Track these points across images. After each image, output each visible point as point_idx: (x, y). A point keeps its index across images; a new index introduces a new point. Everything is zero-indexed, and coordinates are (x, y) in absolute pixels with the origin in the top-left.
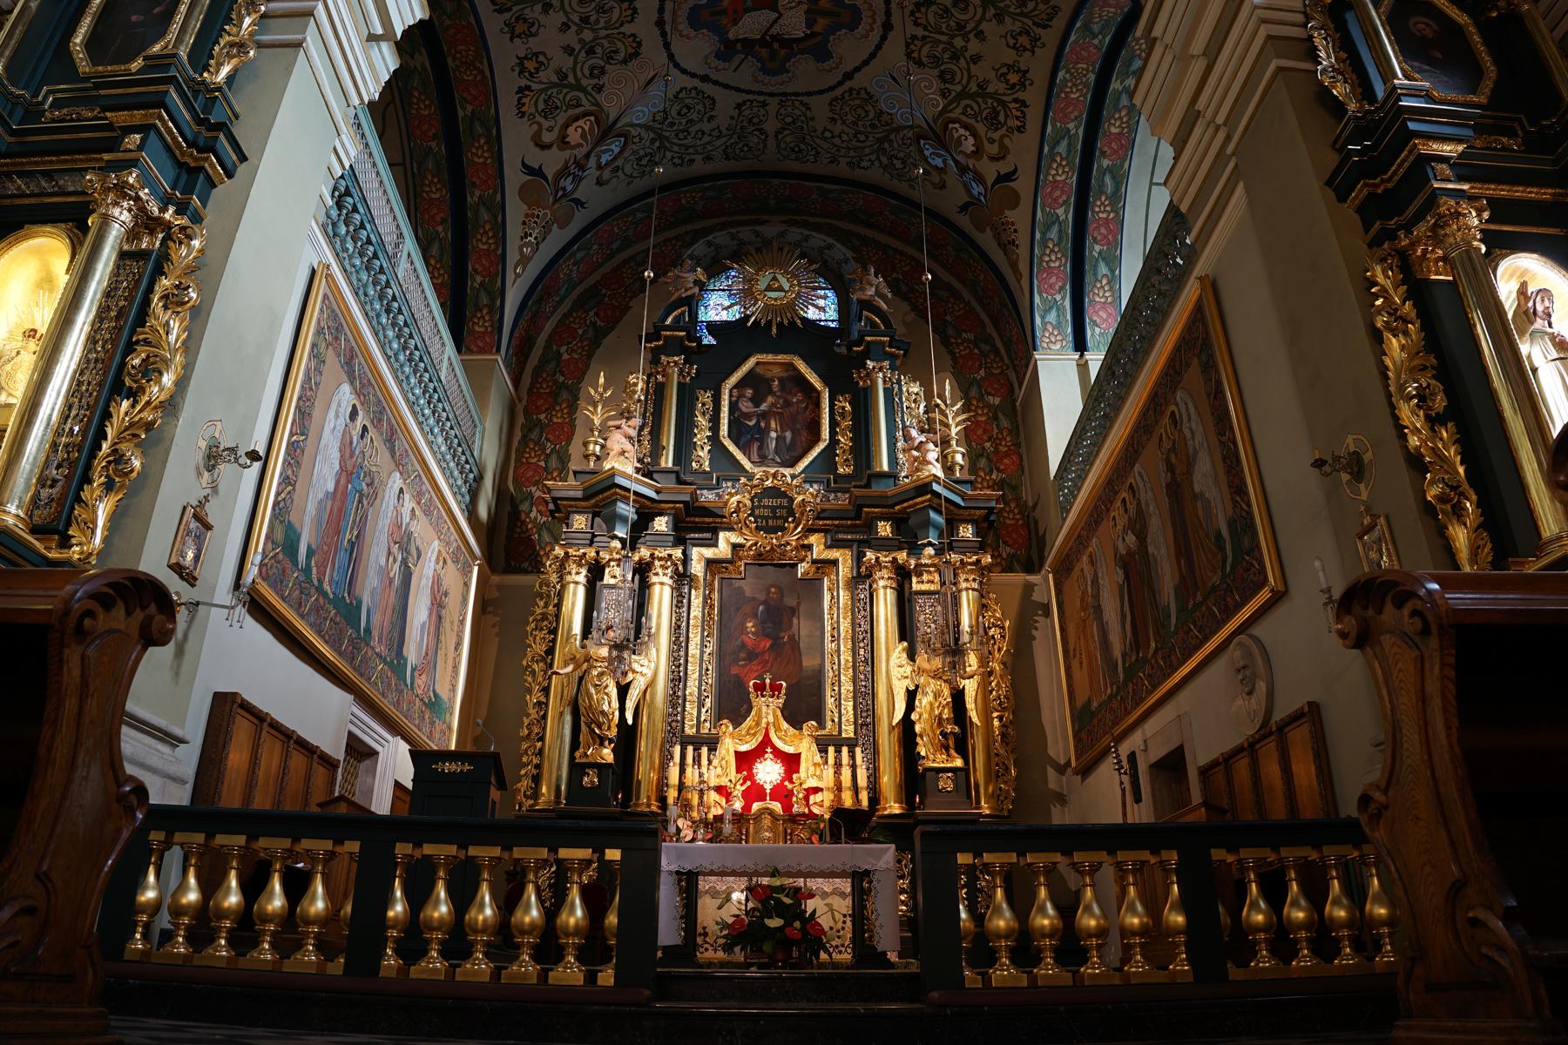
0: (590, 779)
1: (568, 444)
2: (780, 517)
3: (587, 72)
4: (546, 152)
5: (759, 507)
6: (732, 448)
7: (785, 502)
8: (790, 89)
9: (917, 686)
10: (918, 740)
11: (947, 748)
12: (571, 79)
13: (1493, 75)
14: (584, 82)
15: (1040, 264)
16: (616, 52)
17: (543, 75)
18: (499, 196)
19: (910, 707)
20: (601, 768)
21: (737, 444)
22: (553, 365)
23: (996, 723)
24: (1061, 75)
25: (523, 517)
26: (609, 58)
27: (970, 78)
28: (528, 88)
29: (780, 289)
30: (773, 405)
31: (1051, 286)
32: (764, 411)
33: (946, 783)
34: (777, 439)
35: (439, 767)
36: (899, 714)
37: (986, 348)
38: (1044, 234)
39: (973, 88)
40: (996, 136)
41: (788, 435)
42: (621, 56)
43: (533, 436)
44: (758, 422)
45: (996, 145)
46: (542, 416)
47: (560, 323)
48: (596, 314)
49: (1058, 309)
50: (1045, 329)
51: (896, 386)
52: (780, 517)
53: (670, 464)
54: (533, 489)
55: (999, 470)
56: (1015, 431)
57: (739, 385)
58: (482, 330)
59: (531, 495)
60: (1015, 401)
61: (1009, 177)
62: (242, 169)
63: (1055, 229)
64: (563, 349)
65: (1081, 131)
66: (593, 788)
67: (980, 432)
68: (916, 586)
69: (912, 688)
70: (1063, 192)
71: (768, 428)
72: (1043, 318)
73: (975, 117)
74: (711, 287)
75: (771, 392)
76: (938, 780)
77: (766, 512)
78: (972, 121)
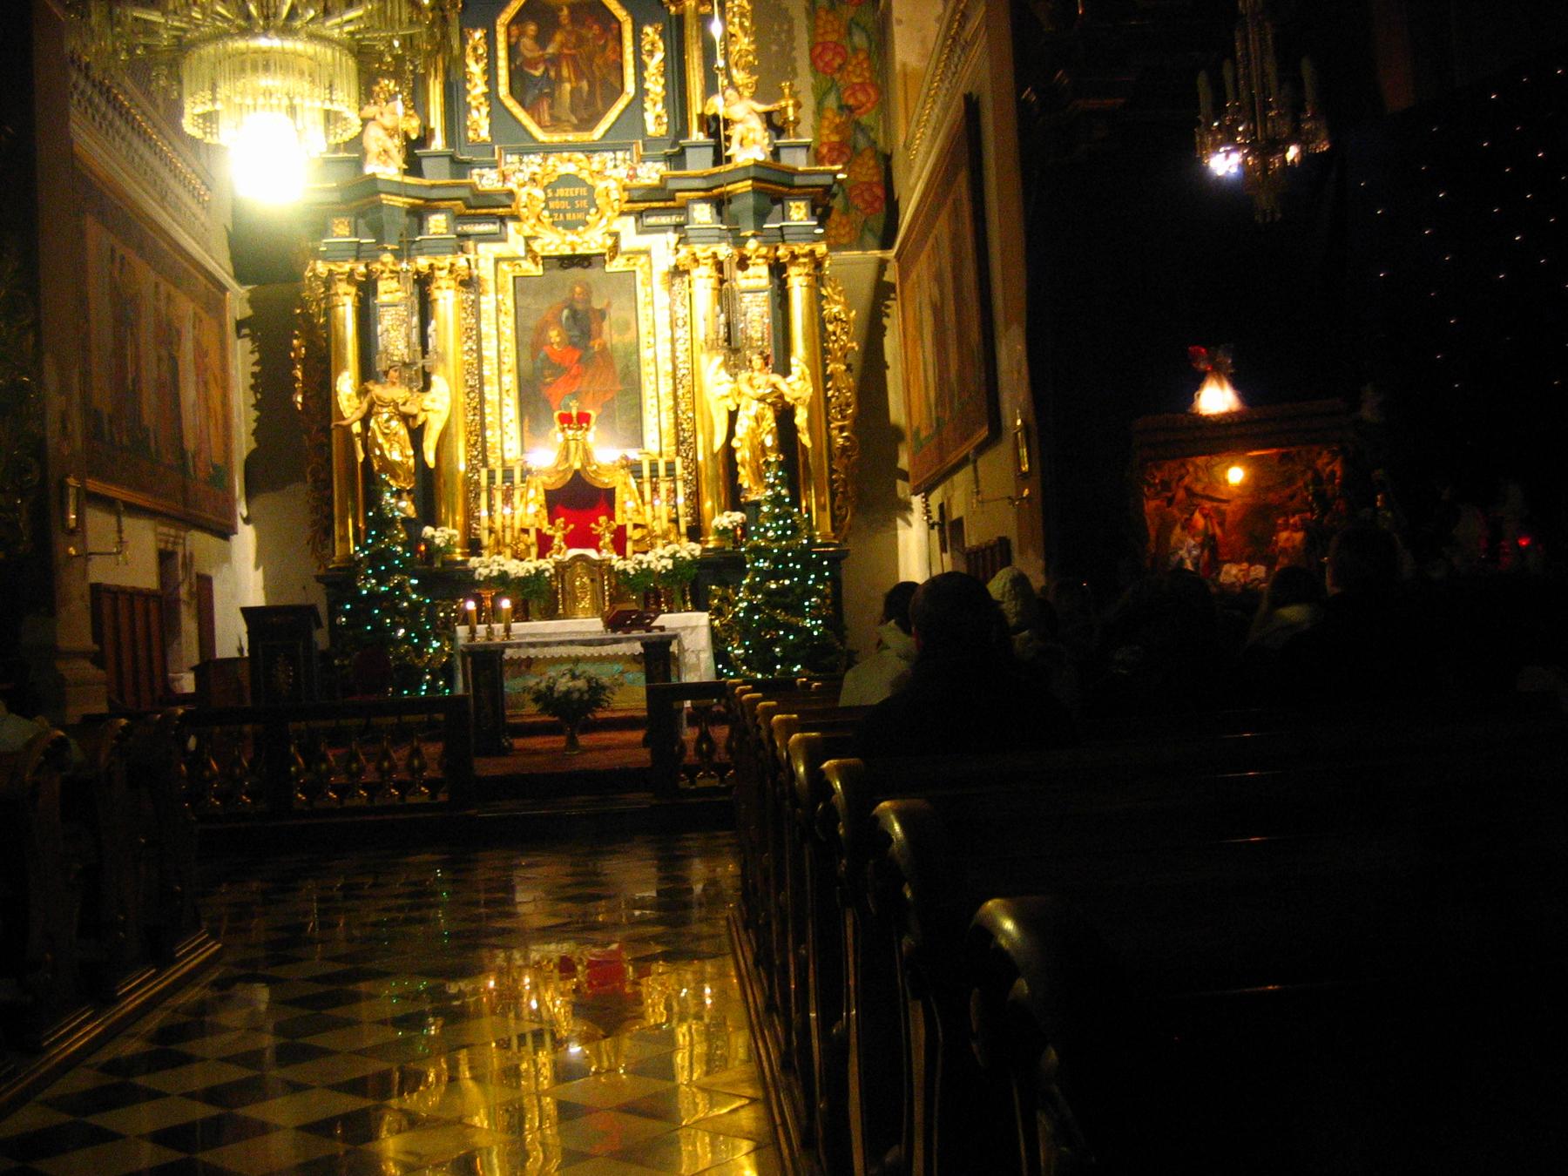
2: (580, 210)
5: (554, 198)
7: (584, 191)
9: (738, 406)
10: (740, 469)
19: (731, 433)
21: (522, 104)
30: (563, 45)
32: (553, 54)
34: (572, 92)
35: (1202, 80)
41: (585, 85)
44: (547, 71)
52: (580, 210)
53: (563, 738)
69: (733, 408)
77: (564, 204)
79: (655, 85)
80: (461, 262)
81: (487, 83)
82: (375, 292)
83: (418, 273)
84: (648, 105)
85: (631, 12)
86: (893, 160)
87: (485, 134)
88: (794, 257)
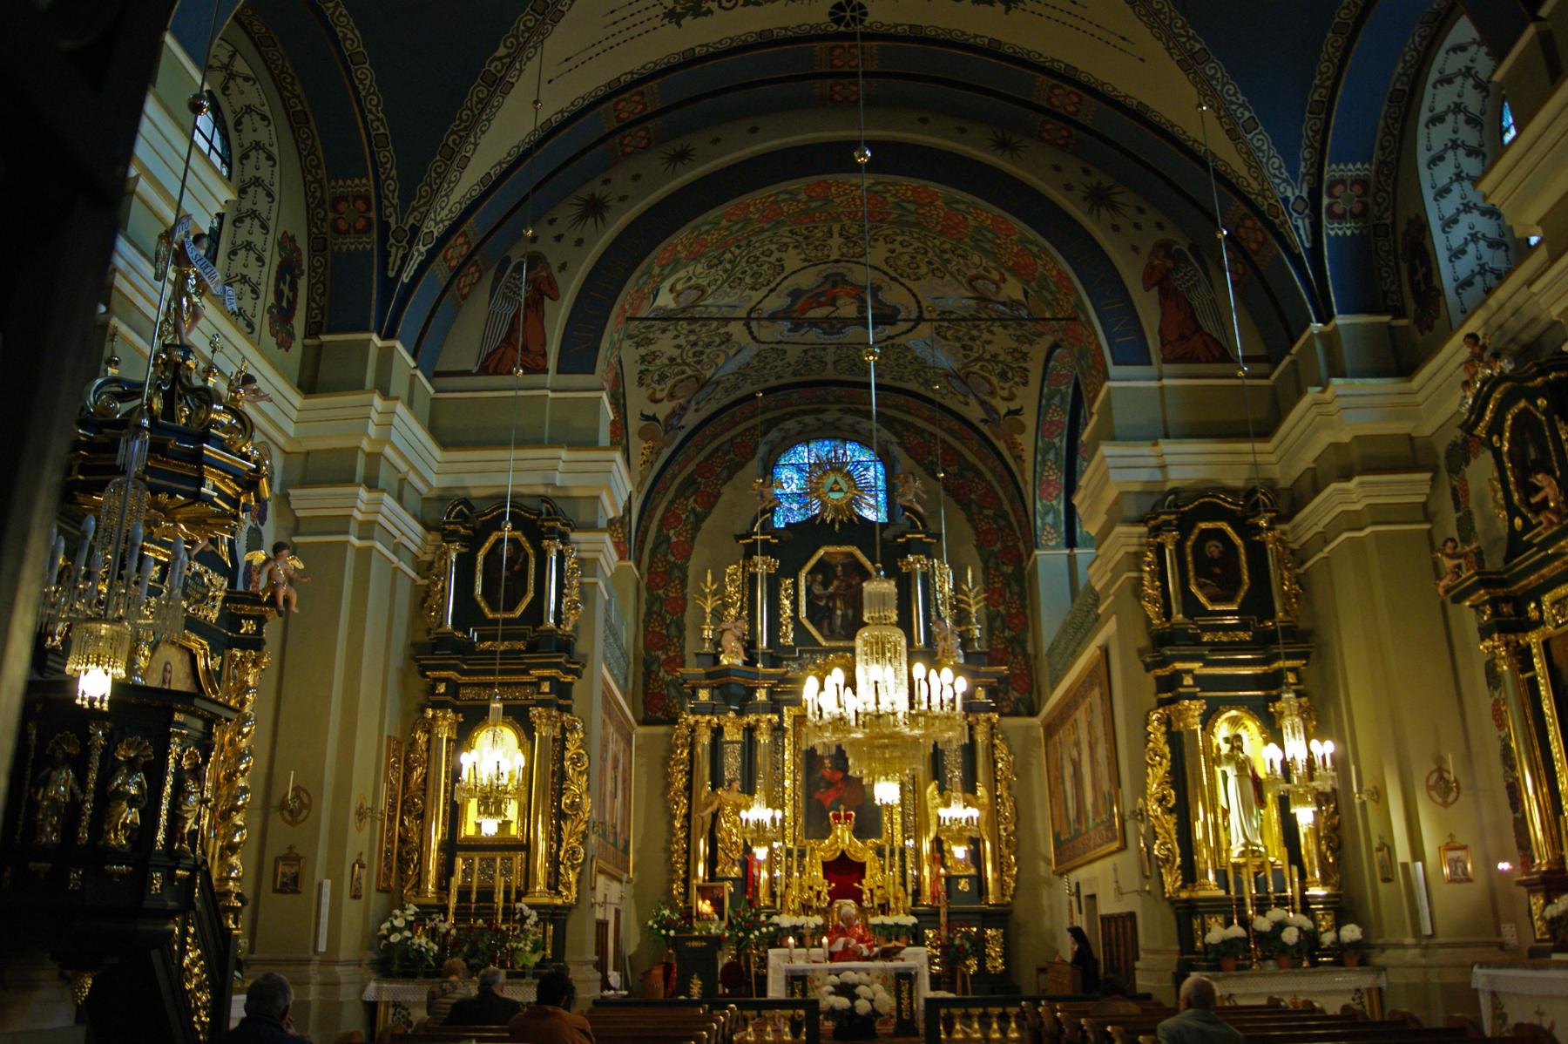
8: (845, 341)
12: (679, 360)
13: (1246, 587)
14: (688, 361)
17: (658, 362)
22: (665, 546)
24: (1052, 364)
26: (708, 345)
29: (840, 490)
30: (838, 588)
31: (1050, 494)
35: (689, 944)
37: (1002, 523)
38: (1043, 457)
40: (1007, 386)
46: (661, 592)
47: (667, 510)
48: (695, 501)
50: (1044, 529)
54: (660, 653)
55: (1010, 629)
56: (1022, 595)
57: (811, 572)
62: (585, 672)
64: (672, 533)
65: (1070, 390)
71: (834, 609)
72: (1042, 519)
73: (990, 372)
74: (782, 462)
75: (836, 577)
76: (958, 884)
81: (792, 611)
83: (748, 724)
87: (790, 641)
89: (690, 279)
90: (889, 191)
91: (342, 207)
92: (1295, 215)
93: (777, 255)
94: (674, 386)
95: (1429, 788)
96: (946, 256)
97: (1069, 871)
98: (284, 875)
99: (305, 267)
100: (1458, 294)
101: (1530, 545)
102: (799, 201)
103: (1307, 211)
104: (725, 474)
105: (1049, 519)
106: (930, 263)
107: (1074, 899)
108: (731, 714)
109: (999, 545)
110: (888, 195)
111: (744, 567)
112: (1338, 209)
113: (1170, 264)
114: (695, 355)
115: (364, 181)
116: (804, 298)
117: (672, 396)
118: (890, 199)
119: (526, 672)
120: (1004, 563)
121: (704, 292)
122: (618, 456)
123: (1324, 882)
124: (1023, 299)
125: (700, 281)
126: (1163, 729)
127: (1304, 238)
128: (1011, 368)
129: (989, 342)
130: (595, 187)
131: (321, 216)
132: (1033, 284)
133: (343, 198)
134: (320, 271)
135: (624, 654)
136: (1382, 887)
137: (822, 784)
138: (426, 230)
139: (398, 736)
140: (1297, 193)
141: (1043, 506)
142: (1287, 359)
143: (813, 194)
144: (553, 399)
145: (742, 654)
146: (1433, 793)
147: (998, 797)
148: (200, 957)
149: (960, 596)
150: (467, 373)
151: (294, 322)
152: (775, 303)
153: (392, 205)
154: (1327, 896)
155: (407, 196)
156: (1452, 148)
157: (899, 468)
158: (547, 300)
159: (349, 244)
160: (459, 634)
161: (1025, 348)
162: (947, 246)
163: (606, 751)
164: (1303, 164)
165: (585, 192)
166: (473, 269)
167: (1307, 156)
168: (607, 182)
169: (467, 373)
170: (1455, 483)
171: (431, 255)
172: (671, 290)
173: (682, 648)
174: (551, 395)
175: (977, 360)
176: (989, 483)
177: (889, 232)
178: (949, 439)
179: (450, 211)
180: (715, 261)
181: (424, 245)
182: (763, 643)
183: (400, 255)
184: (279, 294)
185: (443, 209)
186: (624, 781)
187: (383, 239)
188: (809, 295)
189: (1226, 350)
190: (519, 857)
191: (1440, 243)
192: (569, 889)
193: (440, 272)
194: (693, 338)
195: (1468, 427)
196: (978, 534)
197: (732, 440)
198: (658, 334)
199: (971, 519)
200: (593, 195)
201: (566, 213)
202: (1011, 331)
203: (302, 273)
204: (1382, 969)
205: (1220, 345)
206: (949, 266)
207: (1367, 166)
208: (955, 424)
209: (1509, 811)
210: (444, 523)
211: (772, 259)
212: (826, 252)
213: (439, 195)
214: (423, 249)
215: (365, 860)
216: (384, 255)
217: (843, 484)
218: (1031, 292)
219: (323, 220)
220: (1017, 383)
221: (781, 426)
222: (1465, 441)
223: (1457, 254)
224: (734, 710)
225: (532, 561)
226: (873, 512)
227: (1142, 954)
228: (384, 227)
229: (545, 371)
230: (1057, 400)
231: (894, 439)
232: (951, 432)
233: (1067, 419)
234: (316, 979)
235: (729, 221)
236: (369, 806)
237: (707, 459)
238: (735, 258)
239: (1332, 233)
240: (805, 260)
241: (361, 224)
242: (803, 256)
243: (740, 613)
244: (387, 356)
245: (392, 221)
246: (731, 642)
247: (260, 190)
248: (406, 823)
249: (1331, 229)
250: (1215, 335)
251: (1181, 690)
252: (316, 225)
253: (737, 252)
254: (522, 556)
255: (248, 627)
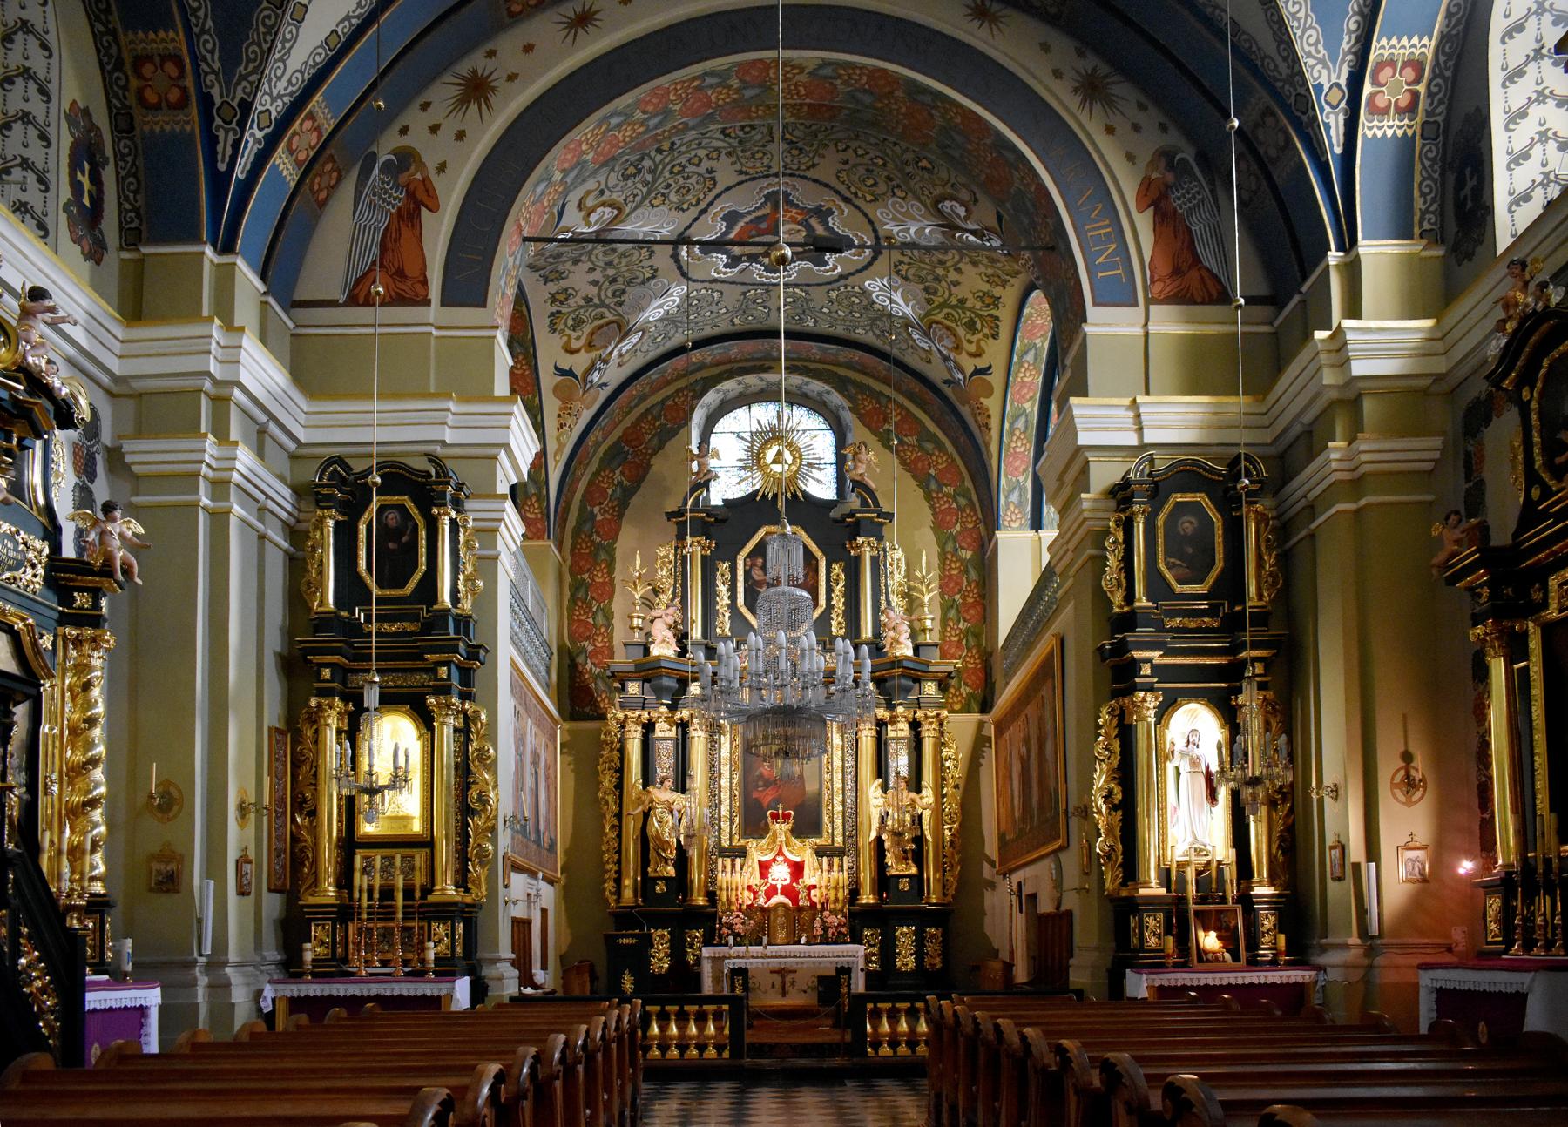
0: (660, 888)
1: (611, 602)
3: (610, 294)
4: (576, 356)
6: (744, 610)
11: (906, 859)
12: (596, 301)
14: (607, 301)
15: (1007, 450)
16: (636, 278)
17: (571, 302)
18: (537, 399)
20: (667, 880)
22: (588, 527)
23: (947, 833)
25: (580, 668)
26: (629, 283)
27: (950, 295)
28: (559, 312)
31: (1016, 469)
33: (904, 885)
36: (873, 835)
37: (963, 501)
38: (1012, 424)
39: (954, 302)
40: (974, 338)
42: (639, 281)
43: (580, 595)
45: (974, 345)
46: (586, 576)
47: (591, 483)
48: (622, 473)
49: (1021, 489)
50: (1008, 508)
51: (882, 553)
54: (586, 643)
55: (965, 620)
58: (533, 516)
59: (584, 649)
60: (985, 554)
61: (984, 371)
63: (1022, 420)
64: (596, 509)
65: (1046, 345)
66: (663, 894)
67: (951, 585)
68: (891, 734)
70: (1030, 389)
72: (1007, 497)
78: (954, 325)
79: (839, 602)
80: (645, 715)
82: (653, 730)
83: (682, 719)
84: (834, 616)
85: (824, 553)
86: (1110, 676)
88: (927, 717)
89: (602, 192)
90: (840, 76)
91: (148, 70)
92: (1328, 109)
93: (706, 164)
94: (592, 334)
95: (1394, 786)
96: (908, 169)
97: (1011, 871)
98: (159, 872)
99: (109, 152)
100: (1510, 211)
101: (1545, 515)
102: (729, 87)
103: (1343, 104)
104: (655, 442)
105: (1014, 497)
106: (889, 178)
107: (1014, 898)
108: (664, 709)
109: (958, 527)
110: (838, 82)
111: (677, 548)
112: (1381, 102)
113: (1170, 178)
114: (614, 295)
115: (171, 34)
116: (741, 224)
117: (590, 346)
118: (841, 88)
119: (420, 657)
120: (962, 548)
121: (620, 210)
122: (518, 410)
123: (1272, 882)
124: (997, 226)
125: (614, 196)
126: (1115, 722)
127: (1334, 141)
128: (981, 316)
129: (956, 284)
130: (477, 61)
131: (122, 83)
132: (1008, 205)
133: (149, 58)
134: (129, 159)
135: (546, 644)
136: (1331, 885)
137: (761, 783)
138: (260, 108)
139: (282, 726)
140: (1334, 79)
141: (1008, 482)
142: (1296, 299)
143: (748, 78)
144: (437, 337)
145: (674, 645)
146: (1397, 792)
147: (944, 796)
148: (39, 960)
149: (912, 583)
150: (333, 304)
151: (104, 225)
152: (712, 228)
153: (213, 72)
154: (1272, 896)
155: (231, 58)
156: (1536, 13)
157: (851, 438)
158: (424, 210)
159: (161, 123)
160: (344, 614)
161: (997, 291)
162: (909, 156)
163: (524, 745)
164: (1346, 38)
165: (464, 68)
166: (329, 167)
167: (1353, 26)
168: (491, 54)
169: (333, 304)
170: (1470, 448)
171: (271, 143)
172: (580, 207)
173: (611, 637)
174: (435, 333)
175: (942, 306)
176: (950, 456)
177: (840, 135)
178: (908, 404)
179: (289, 81)
180: (632, 170)
181: (261, 129)
182: (696, 634)
183: (230, 141)
184: (76, 187)
185: (279, 79)
186: (547, 778)
187: (207, 119)
188: (748, 219)
189: (1224, 288)
190: (420, 858)
191: (1501, 143)
192: (479, 886)
193: (284, 164)
194: (611, 272)
195: (1495, 379)
196: (935, 514)
197: (663, 401)
198: (568, 265)
199: (928, 497)
200: (475, 72)
201: (443, 93)
202: (982, 269)
203: (106, 162)
204: (1321, 969)
205: (1219, 281)
206: (912, 183)
207: (1425, 40)
208: (916, 387)
209: (1478, 811)
210: (318, 486)
211: (702, 170)
212: (766, 162)
213: (271, 60)
214: (260, 135)
215: (251, 854)
216: (211, 141)
217: (788, 456)
218: (1006, 217)
219: (125, 88)
220: (986, 336)
221: (719, 387)
222: (1490, 395)
223: (1520, 158)
224: (667, 705)
225: (423, 534)
226: (822, 487)
227: (1076, 951)
228: (206, 101)
229: (426, 302)
230: (1030, 357)
231: (846, 404)
232: (911, 396)
233: (1041, 379)
234: (203, 981)
235: (644, 112)
236: (253, 801)
237: (635, 425)
238: (657, 166)
239: (1369, 134)
240: (741, 172)
241: (174, 95)
242: (738, 166)
243: (673, 599)
244: (226, 277)
245: (215, 92)
246: (661, 631)
247: (31, 38)
248: (298, 820)
249: (1371, 128)
250: (1215, 271)
251: (1137, 680)
252: (116, 96)
253: (658, 158)
254: (410, 524)
255: (81, 600)
